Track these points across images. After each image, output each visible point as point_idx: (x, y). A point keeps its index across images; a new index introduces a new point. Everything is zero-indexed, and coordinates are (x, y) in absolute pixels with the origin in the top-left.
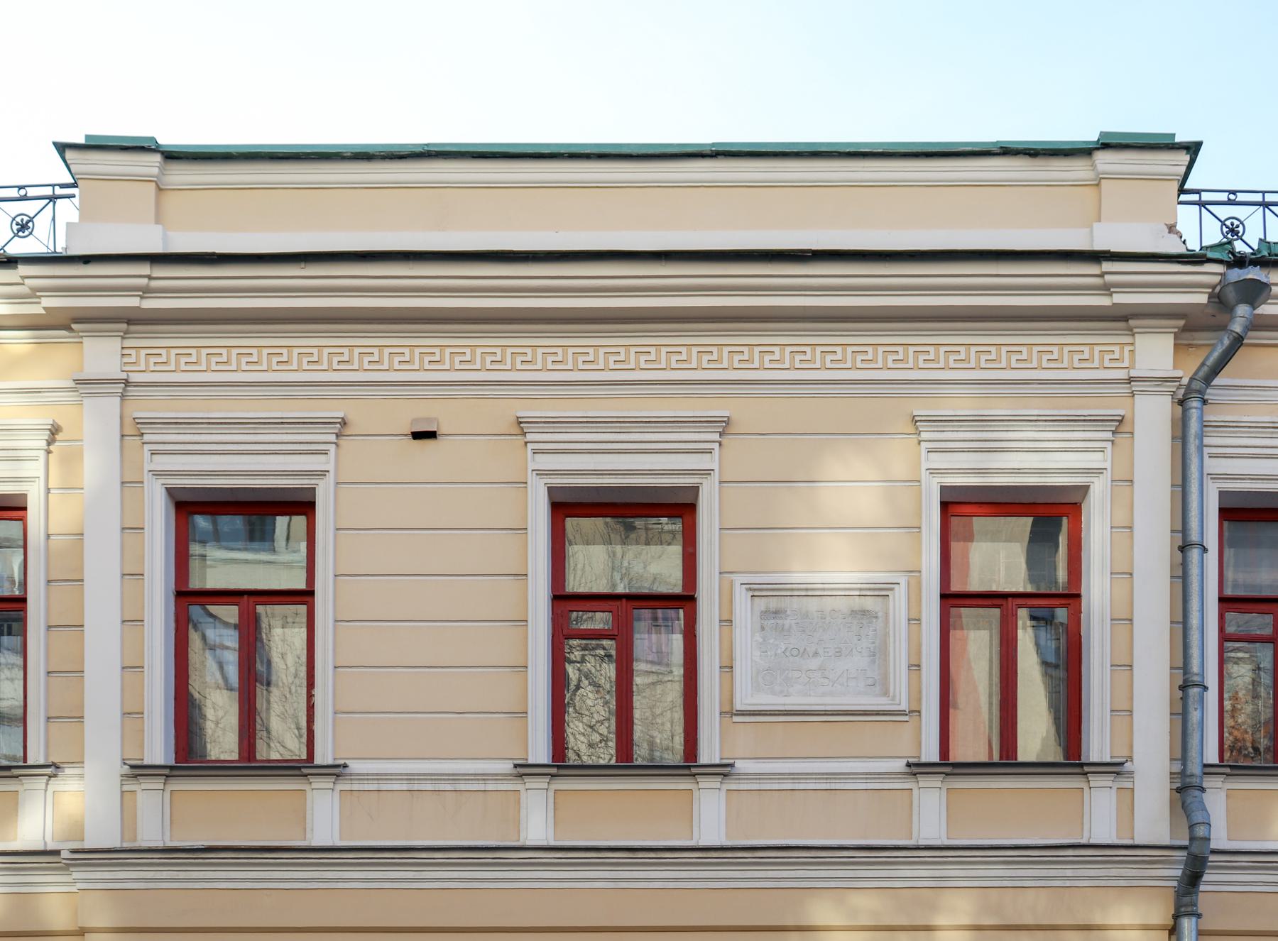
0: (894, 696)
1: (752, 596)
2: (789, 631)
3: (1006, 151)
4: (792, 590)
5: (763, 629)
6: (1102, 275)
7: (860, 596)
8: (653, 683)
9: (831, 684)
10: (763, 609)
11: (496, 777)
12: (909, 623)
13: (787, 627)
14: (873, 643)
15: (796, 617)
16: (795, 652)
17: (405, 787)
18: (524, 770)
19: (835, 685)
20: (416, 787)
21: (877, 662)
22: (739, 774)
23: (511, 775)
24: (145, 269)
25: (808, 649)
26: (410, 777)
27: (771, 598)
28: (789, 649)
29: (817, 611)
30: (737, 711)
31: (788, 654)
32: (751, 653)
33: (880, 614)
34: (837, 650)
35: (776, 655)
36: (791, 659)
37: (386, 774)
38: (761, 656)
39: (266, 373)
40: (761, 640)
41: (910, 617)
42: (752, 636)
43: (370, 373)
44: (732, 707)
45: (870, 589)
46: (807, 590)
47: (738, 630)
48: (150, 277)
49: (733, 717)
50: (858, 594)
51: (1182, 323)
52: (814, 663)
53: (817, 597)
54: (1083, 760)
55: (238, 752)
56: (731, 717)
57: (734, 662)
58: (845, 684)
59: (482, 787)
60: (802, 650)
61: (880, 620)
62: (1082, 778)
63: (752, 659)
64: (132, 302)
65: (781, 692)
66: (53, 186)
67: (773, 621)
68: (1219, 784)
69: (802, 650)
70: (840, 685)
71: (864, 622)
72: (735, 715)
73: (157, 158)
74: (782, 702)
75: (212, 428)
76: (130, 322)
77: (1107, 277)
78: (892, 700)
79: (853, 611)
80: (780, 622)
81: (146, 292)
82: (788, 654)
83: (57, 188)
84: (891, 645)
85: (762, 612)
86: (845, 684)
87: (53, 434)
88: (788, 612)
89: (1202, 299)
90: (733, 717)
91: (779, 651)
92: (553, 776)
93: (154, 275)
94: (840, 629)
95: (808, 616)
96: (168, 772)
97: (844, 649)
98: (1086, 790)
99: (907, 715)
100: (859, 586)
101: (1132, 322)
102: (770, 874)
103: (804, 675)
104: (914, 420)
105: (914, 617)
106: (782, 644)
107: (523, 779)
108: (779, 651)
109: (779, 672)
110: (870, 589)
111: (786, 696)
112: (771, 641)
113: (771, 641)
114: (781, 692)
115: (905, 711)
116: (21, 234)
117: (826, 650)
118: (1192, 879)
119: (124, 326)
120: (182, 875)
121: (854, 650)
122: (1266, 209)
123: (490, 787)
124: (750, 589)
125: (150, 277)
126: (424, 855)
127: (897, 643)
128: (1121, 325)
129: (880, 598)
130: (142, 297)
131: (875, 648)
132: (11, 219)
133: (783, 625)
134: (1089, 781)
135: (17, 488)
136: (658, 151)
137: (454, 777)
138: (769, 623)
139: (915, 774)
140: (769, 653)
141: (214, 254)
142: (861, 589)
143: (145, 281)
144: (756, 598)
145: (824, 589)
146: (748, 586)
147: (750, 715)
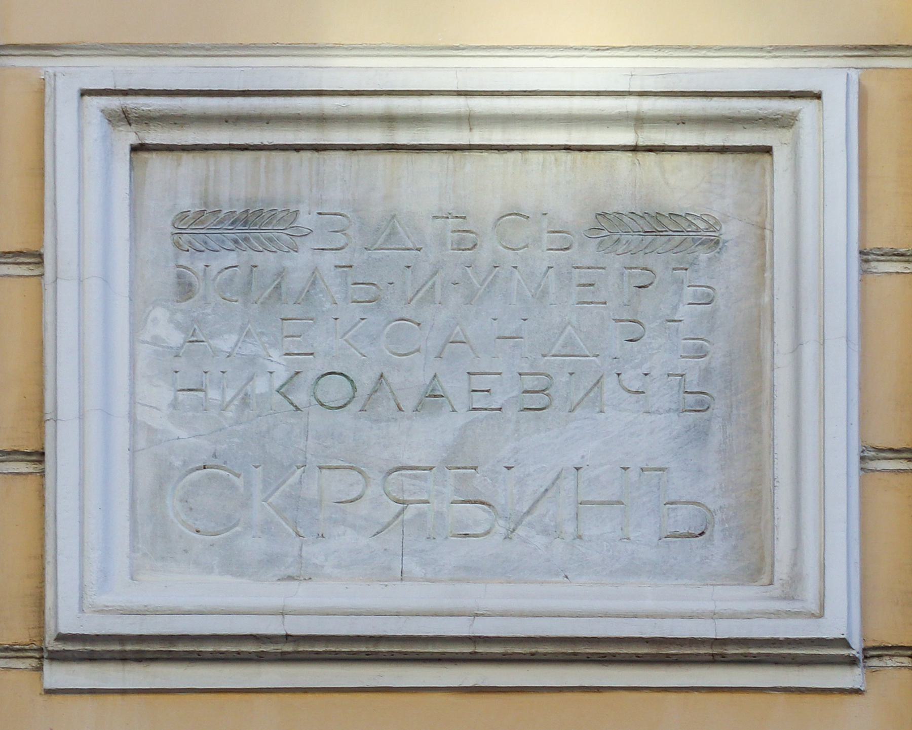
0: (796, 578)
1: (135, 149)
2: (307, 296)
4: (321, 120)
7: (635, 149)
8: (398, 222)
9: (501, 527)
10: (187, 203)
12: (864, 272)
13: (297, 281)
14: (701, 353)
15: (340, 239)
16: (335, 390)
19: (521, 531)
21: (716, 438)
25: (394, 378)
27: (225, 158)
28: (310, 376)
29: (454, 232)
30: (61, 638)
31: (301, 397)
32: (132, 394)
33: (730, 231)
34: (530, 383)
35: (245, 401)
36: (317, 418)
38: (174, 405)
40: (176, 338)
41: (873, 243)
42: (136, 325)
44: (41, 626)
45: (682, 121)
46: (390, 120)
47: (67, 291)
49: (47, 667)
50: (626, 137)
53: (437, 157)
55: (727, 144)
56: (40, 669)
57: (49, 426)
58: (570, 528)
60: (366, 382)
61: (730, 256)
63: (132, 418)
65: (271, 560)
67: (231, 258)
69: (364, 389)
70: (545, 532)
71: (655, 262)
72: (58, 657)
74: (276, 602)
78: (786, 598)
79: (604, 215)
80: (267, 261)
82: (301, 397)
84: (783, 360)
85: (183, 216)
86: (570, 528)
87: (298, 185)
88: (305, 220)
90: (47, 667)
91: (261, 386)
94: (543, 294)
95: (393, 233)
97: (562, 379)
99: (852, 662)
100: (632, 105)
103: (375, 490)
105: (887, 246)
106: (275, 354)
108: (261, 386)
109: (258, 475)
110: (682, 121)
111: (291, 578)
112: (226, 343)
113: (226, 343)
114: (271, 560)
115: (844, 643)
117: (479, 382)
121: (610, 383)
124: (127, 118)
127: (809, 351)
129: (730, 162)
131: (706, 374)
133: (281, 274)
138: (216, 266)
140: (213, 394)
142: (639, 121)
144: (155, 161)
145: (469, 120)
146: (115, 102)
147: (123, 658)
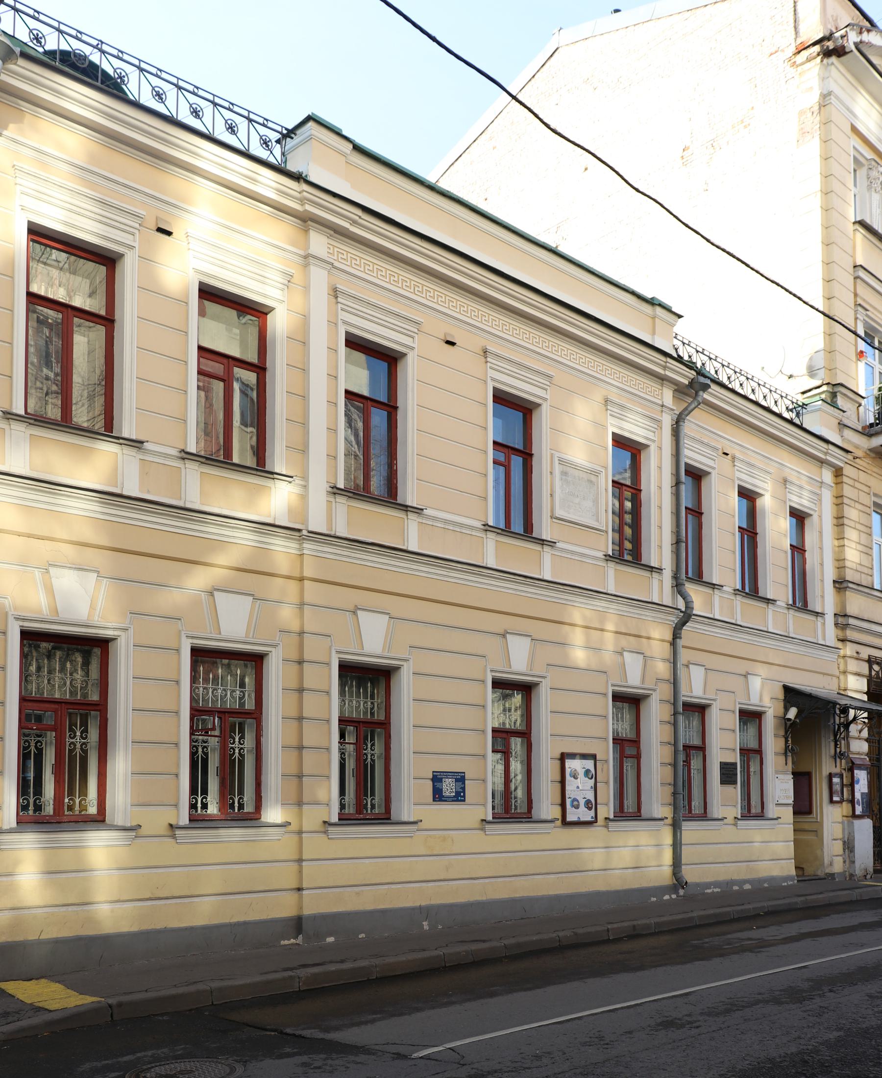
0: (601, 522)
3: (633, 293)
5: (562, 480)
6: (666, 362)
11: (166, 456)
17: (443, 526)
18: (487, 528)
20: (447, 527)
22: (426, 515)
23: (482, 529)
24: (359, 212)
26: (446, 521)
37: (437, 518)
39: (387, 283)
43: (367, 275)
48: (360, 217)
51: (676, 388)
52: (577, 500)
54: (267, 469)
59: (470, 533)
62: (404, 513)
64: (346, 225)
66: (282, 127)
68: (415, 518)
73: (351, 146)
75: (127, 216)
76: (336, 231)
77: (668, 364)
81: (354, 222)
83: (284, 129)
89: (687, 382)
92: (498, 533)
93: (362, 217)
96: (207, 460)
98: (334, 503)
101: (665, 382)
102: (393, 563)
104: (607, 401)
107: (9, 422)
116: (270, 147)
118: (683, 623)
119: (332, 233)
120: (353, 555)
122: (247, 149)
123: (474, 533)
125: (360, 217)
126: (559, 586)
128: (660, 381)
130: (351, 224)
132: (44, 35)
134: (10, 425)
135: (264, 301)
136: (533, 239)
137: (461, 525)
139: (335, 494)
141: (394, 220)
142: (591, 471)
143: (357, 218)
